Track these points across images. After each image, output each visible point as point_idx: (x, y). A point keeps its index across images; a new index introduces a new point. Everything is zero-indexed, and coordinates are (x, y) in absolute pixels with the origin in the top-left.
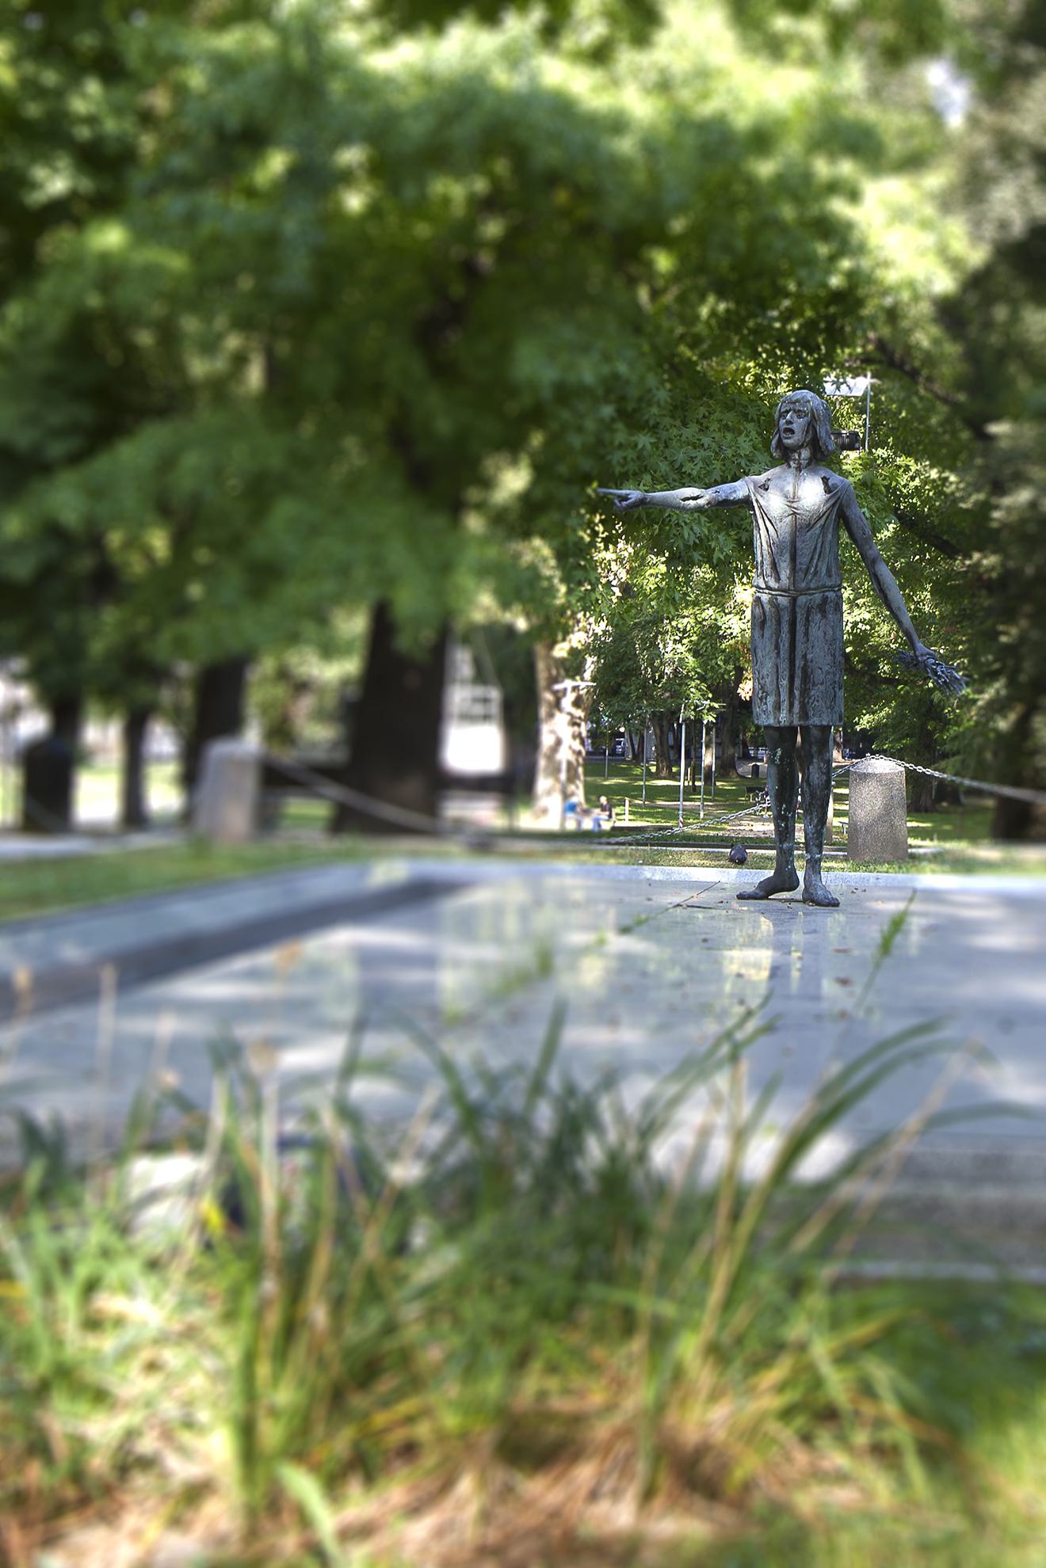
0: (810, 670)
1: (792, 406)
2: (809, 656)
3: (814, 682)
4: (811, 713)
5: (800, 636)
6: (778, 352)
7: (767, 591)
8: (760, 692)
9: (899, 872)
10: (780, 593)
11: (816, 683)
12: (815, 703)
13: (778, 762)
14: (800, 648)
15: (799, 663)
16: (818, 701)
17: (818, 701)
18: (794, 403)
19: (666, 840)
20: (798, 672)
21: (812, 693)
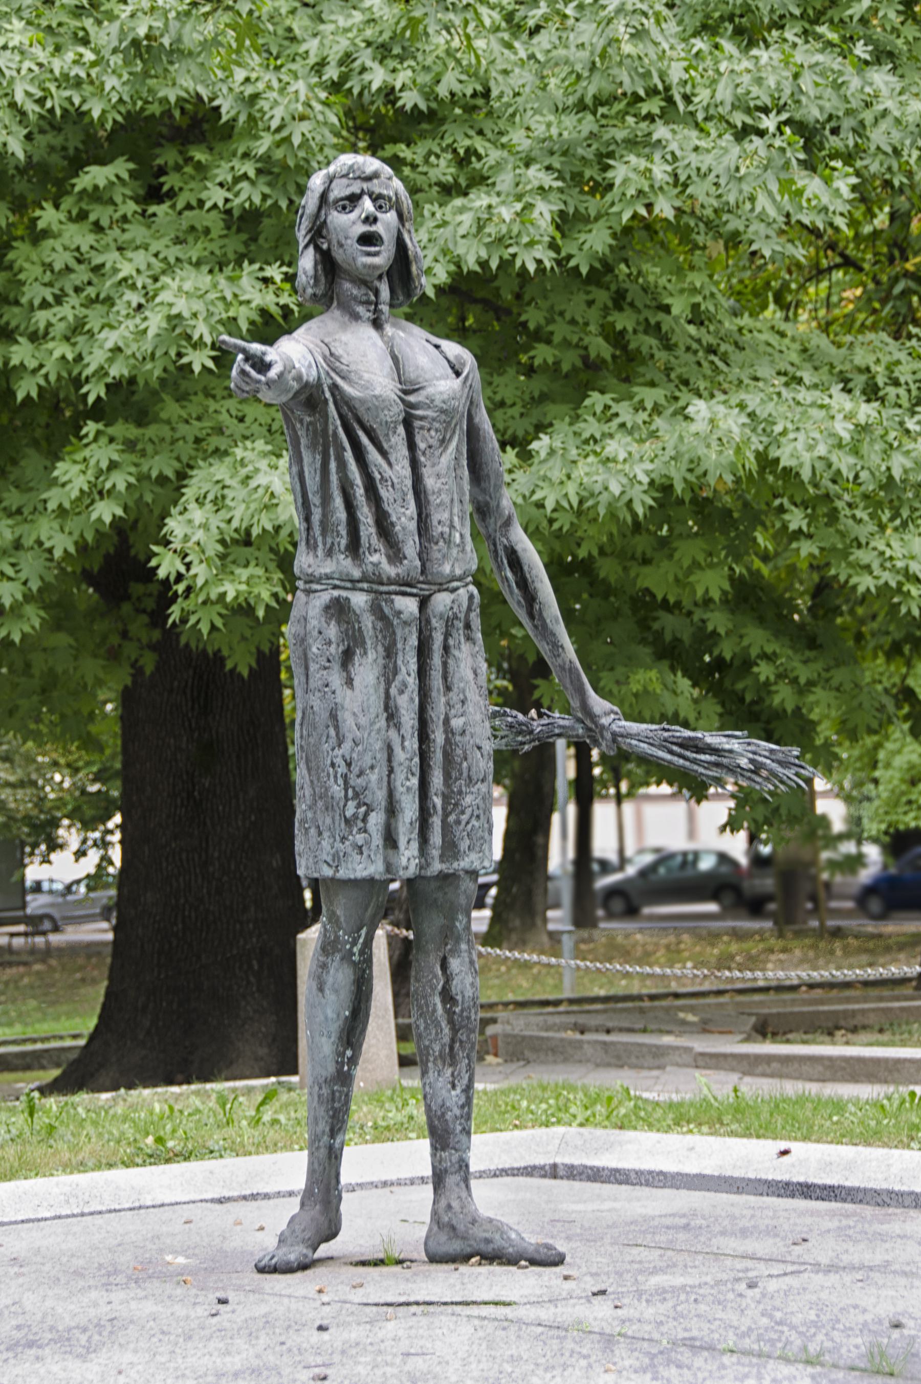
0: (459, 752)
1: (365, 186)
2: (456, 723)
3: (469, 777)
4: (464, 845)
5: (436, 681)
6: (68, 414)
7: (365, 586)
8: (351, 805)
9: (909, 1147)
10: (397, 588)
11: (475, 778)
12: (474, 822)
13: (356, 958)
14: (437, 711)
15: (438, 737)
16: (478, 817)
17: (478, 817)
18: (369, 179)
19: (279, 1083)
20: (437, 758)
21: (468, 799)
